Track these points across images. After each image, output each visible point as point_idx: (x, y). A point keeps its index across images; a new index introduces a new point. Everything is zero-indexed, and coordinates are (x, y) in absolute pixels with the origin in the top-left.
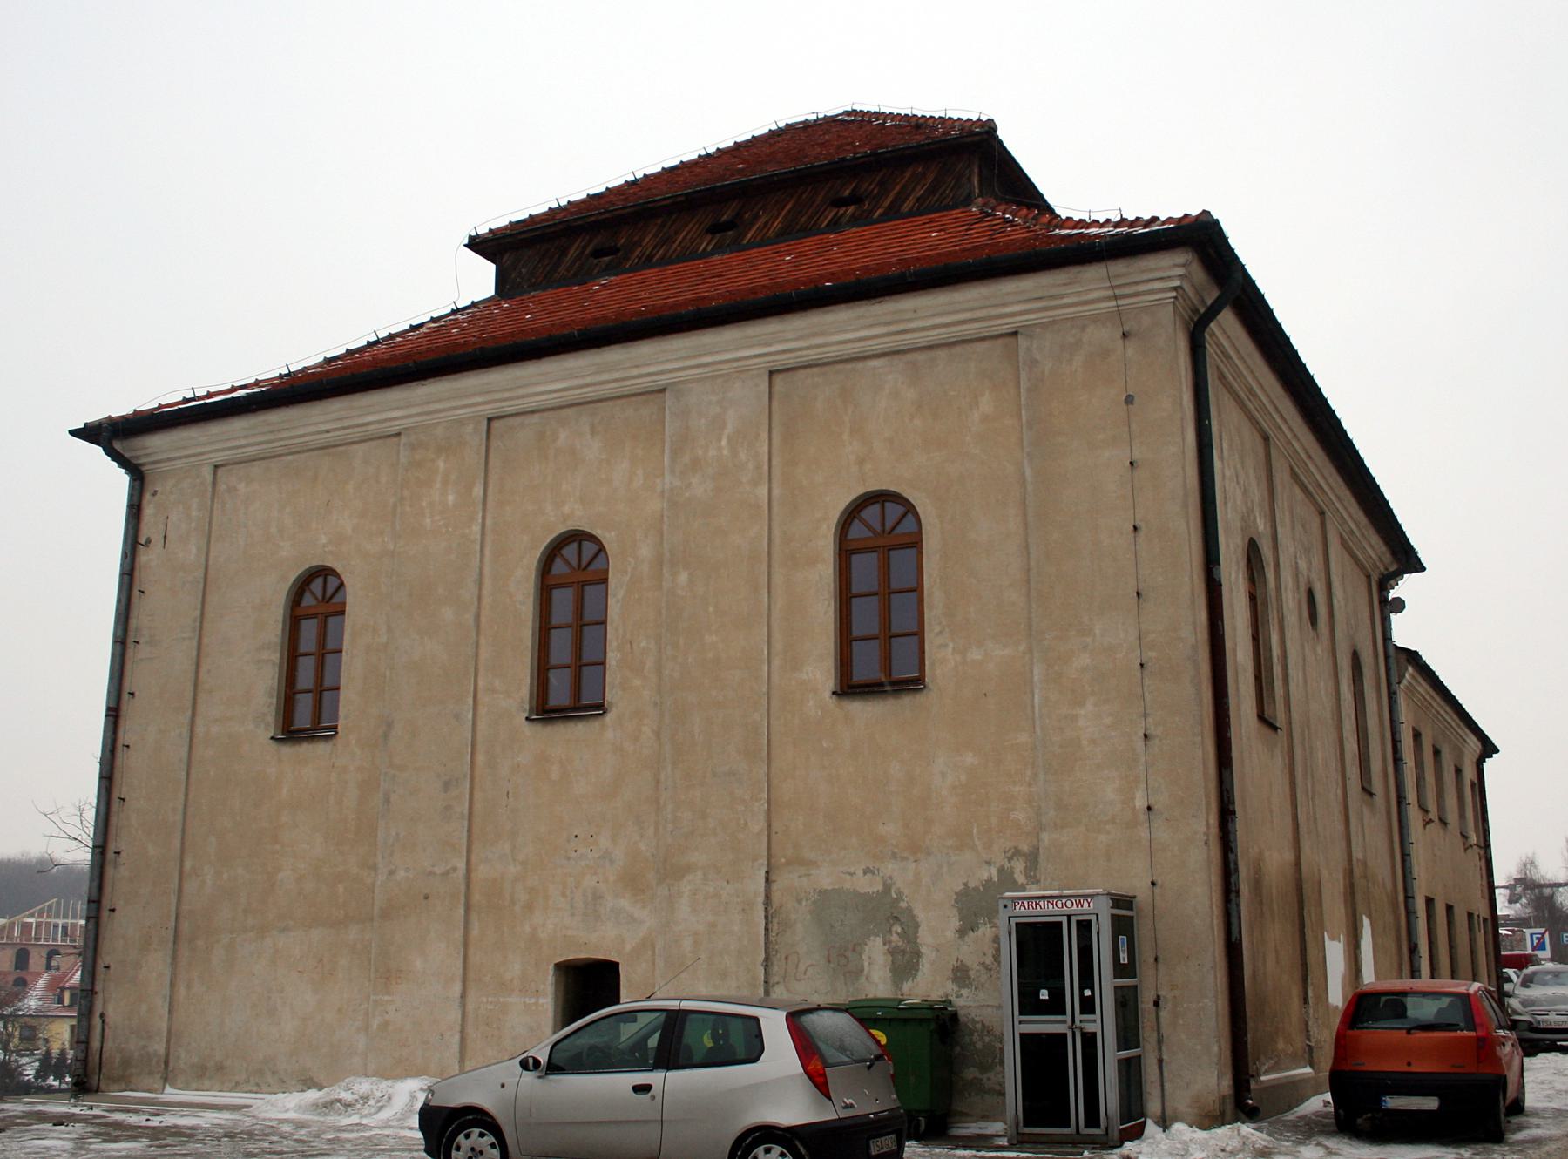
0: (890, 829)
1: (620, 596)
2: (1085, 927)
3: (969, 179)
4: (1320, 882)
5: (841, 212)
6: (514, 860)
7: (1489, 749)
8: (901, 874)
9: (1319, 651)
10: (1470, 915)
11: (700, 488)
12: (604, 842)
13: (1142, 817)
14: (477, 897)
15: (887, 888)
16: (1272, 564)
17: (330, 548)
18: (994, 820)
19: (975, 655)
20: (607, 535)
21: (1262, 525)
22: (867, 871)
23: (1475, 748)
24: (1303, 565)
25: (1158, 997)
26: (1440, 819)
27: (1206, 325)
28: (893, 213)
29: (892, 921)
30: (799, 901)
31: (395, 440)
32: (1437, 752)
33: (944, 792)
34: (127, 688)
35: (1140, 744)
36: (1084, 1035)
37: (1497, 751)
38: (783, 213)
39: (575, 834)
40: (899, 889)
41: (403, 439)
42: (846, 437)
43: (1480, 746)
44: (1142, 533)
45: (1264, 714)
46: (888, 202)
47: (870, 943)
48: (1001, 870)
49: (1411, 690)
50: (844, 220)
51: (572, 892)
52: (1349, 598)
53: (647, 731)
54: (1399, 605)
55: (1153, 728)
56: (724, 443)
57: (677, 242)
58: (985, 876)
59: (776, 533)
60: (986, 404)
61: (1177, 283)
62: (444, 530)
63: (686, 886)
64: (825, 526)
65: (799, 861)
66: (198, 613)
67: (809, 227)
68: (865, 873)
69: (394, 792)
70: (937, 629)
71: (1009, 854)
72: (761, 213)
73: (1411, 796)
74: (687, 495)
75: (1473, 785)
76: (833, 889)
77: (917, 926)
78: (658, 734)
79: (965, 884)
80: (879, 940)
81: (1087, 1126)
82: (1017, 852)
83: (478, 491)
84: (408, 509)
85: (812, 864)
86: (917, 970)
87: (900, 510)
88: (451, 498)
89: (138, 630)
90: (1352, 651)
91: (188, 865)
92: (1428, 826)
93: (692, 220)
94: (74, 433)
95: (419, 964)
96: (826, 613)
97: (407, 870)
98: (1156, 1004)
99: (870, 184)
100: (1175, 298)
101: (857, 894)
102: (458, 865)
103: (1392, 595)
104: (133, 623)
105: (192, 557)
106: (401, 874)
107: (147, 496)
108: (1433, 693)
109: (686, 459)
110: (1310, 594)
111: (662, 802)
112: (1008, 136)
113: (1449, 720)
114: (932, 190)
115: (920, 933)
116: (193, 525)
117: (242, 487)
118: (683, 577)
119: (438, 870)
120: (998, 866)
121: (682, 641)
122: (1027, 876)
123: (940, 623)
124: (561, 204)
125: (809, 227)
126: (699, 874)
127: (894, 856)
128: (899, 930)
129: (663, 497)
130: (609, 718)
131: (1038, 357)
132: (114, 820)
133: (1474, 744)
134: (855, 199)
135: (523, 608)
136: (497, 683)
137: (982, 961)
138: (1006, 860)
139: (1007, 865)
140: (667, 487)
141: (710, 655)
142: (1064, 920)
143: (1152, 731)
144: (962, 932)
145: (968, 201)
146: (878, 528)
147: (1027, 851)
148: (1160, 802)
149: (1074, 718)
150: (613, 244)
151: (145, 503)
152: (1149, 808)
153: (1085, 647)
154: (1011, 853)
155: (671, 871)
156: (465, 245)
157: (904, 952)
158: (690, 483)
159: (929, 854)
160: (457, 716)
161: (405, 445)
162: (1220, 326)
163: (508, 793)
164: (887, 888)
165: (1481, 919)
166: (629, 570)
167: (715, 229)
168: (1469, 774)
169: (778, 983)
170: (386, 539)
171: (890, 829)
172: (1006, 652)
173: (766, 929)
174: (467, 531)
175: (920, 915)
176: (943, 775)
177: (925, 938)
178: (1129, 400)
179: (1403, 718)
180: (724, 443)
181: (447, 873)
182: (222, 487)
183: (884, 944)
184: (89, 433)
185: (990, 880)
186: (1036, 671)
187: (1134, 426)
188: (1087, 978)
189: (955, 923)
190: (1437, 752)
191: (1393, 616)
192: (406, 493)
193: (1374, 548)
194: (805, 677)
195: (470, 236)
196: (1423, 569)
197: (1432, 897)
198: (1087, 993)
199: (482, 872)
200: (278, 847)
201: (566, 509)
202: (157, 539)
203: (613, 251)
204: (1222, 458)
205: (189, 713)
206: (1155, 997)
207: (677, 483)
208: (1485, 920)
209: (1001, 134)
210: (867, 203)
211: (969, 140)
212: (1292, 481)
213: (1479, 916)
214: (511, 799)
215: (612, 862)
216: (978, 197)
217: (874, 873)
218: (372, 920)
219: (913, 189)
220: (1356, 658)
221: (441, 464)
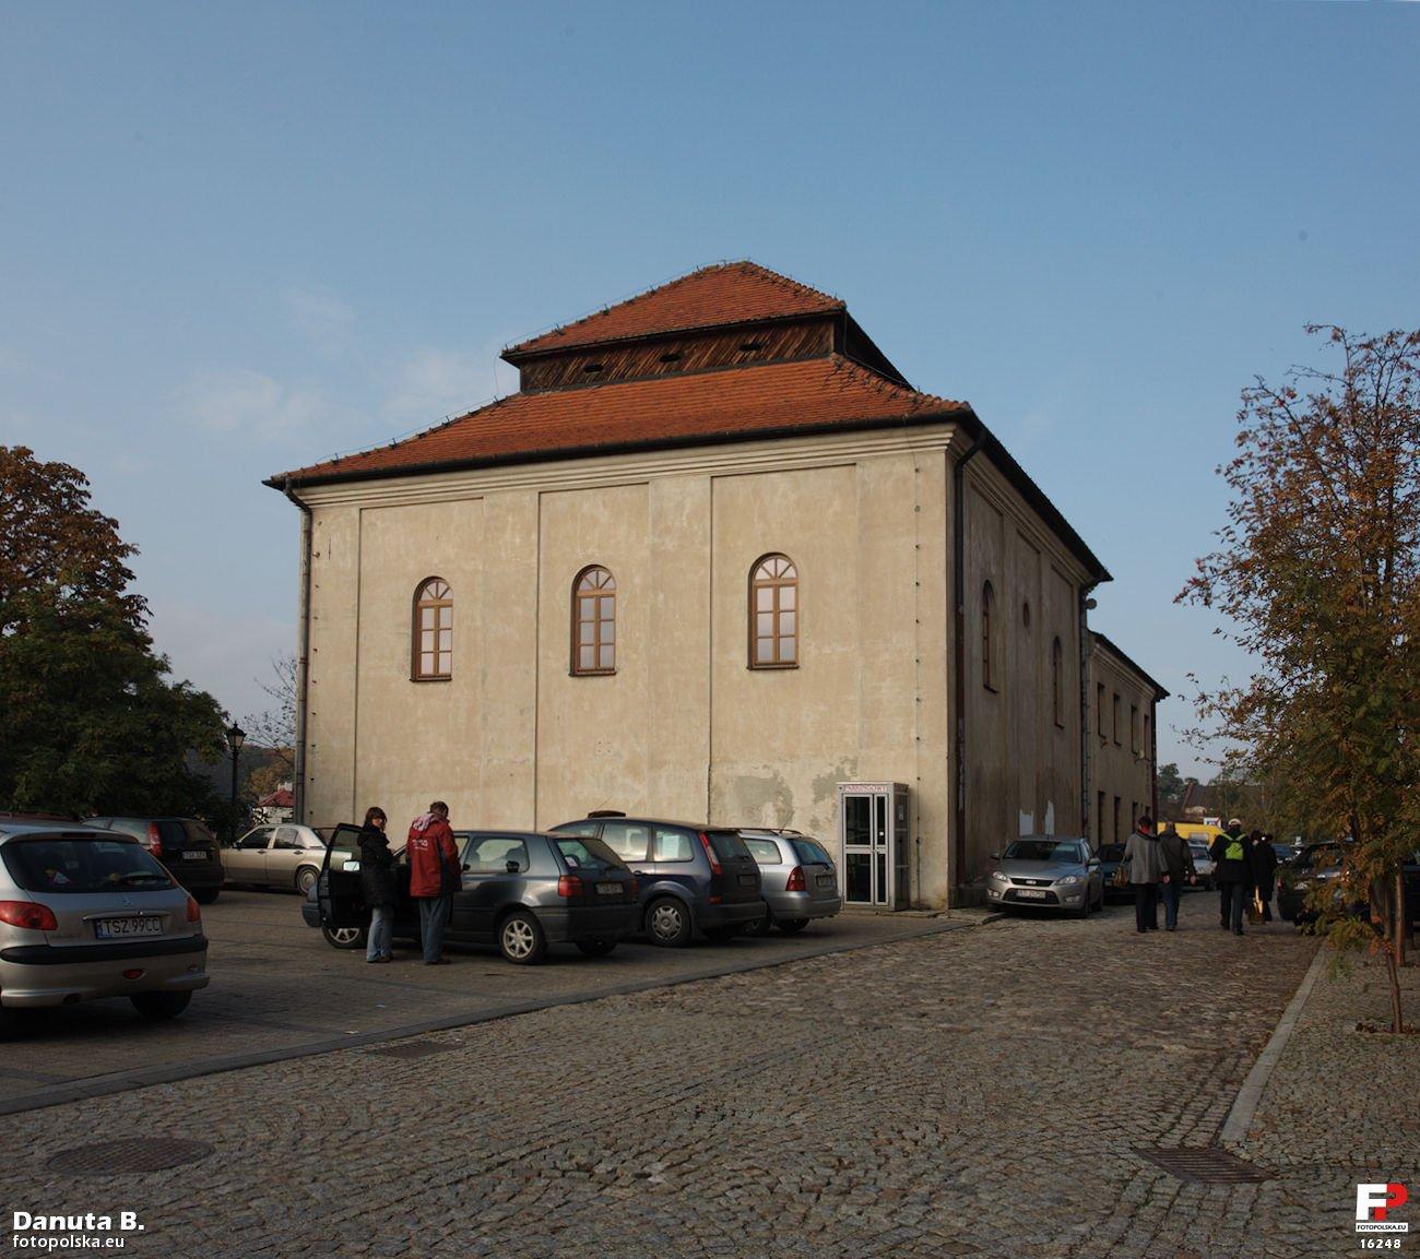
1: (624, 605)
2: (881, 801)
3: (828, 339)
7: (1161, 693)
10: (1135, 805)
11: (670, 544)
13: (914, 742)
15: (776, 776)
16: (1000, 593)
17: (441, 566)
19: (827, 650)
22: (765, 767)
24: (1022, 590)
27: (965, 462)
30: (727, 782)
32: (1116, 698)
34: (312, 645)
35: (914, 703)
36: (879, 855)
38: (710, 352)
42: (755, 520)
45: (988, 681)
46: (776, 350)
48: (838, 769)
50: (748, 360)
52: (1053, 596)
54: (1093, 604)
56: (684, 518)
58: (829, 772)
60: (837, 505)
61: (948, 442)
66: (356, 601)
70: (806, 635)
73: (1092, 727)
75: (1146, 717)
77: (791, 797)
80: (771, 804)
81: (879, 901)
82: (847, 759)
83: (534, 537)
84: (490, 545)
87: (786, 564)
88: (518, 540)
89: (316, 610)
90: (1053, 639)
91: (359, 753)
94: (263, 482)
95: (508, 813)
98: (918, 841)
101: (760, 780)
104: (313, 606)
106: (495, 762)
107: (315, 525)
110: (1026, 606)
112: (855, 312)
114: (802, 346)
115: (793, 801)
116: (348, 546)
117: (379, 524)
118: (661, 597)
127: (779, 759)
131: (867, 479)
132: (309, 726)
139: (841, 767)
141: (677, 643)
142: (871, 797)
143: (920, 698)
144: (815, 801)
145: (826, 353)
146: (773, 574)
148: (924, 735)
151: (314, 530)
153: (887, 650)
155: (656, 764)
160: (527, 673)
162: (974, 461)
164: (776, 776)
167: (666, 359)
168: (1143, 710)
172: (844, 650)
176: (808, 716)
177: (796, 803)
180: (684, 518)
181: (523, 762)
182: (365, 523)
184: (276, 483)
185: (832, 773)
188: (881, 826)
189: (813, 796)
190: (1116, 698)
191: (1088, 611)
193: (1076, 568)
196: (1112, 579)
198: (882, 834)
202: (324, 554)
203: (599, 368)
204: (970, 537)
205: (355, 663)
209: (849, 310)
215: (621, 757)
220: (1057, 642)
221: (510, 519)
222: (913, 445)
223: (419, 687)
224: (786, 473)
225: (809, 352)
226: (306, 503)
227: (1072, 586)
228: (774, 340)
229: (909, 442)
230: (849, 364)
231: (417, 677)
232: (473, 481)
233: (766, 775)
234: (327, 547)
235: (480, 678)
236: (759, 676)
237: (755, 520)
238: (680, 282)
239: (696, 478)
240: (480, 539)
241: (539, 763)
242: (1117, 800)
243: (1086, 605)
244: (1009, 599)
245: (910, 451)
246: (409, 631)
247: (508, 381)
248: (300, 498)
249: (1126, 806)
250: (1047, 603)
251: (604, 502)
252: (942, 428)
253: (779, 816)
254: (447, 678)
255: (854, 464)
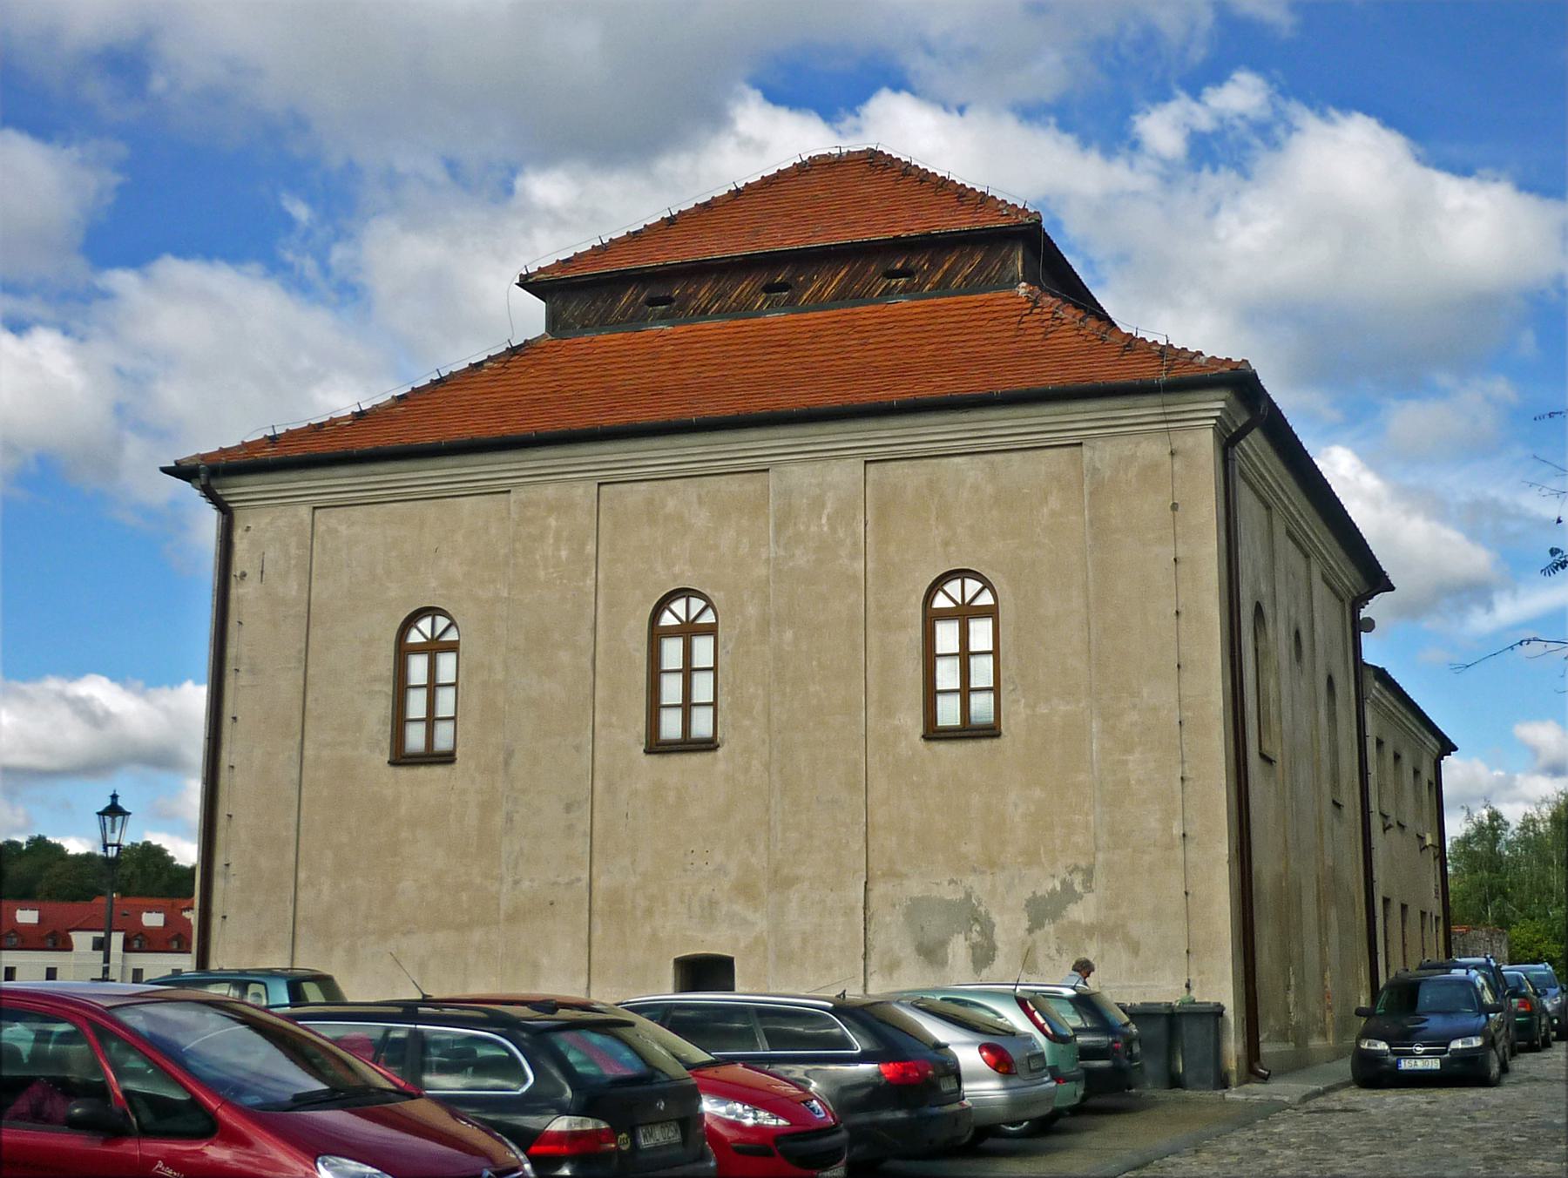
0: (971, 848)
4: (1300, 887)
5: (893, 283)
6: (634, 871)
7: (1448, 747)
8: (978, 885)
9: (1302, 684)
10: (1423, 914)
12: (719, 857)
13: (1179, 842)
14: (599, 903)
15: (969, 896)
18: (1058, 842)
19: (1043, 709)
20: (716, 594)
21: (1264, 588)
22: (951, 882)
23: (1433, 748)
25: (1189, 980)
26: (1399, 824)
28: (942, 288)
29: (972, 922)
31: (505, 495)
32: (1397, 757)
33: (1017, 819)
37: (1455, 749)
39: (692, 849)
40: (978, 896)
41: (513, 497)
42: (932, 522)
43: (1439, 747)
44: (1182, 617)
47: (954, 940)
48: (1063, 882)
49: (1377, 704)
51: (690, 898)
52: (1327, 620)
53: (756, 764)
54: (1369, 625)
55: (1188, 771)
56: (824, 520)
57: (732, 299)
58: (1050, 887)
59: (870, 599)
61: (1218, 414)
62: (558, 582)
63: (794, 895)
64: (914, 597)
65: (892, 874)
66: (304, 645)
67: (862, 295)
68: (949, 884)
69: (517, 812)
71: (1069, 869)
72: (815, 277)
74: (791, 564)
75: (1430, 783)
76: (923, 897)
78: (767, 767)
79: (1034, 893)
80: (961, 937)
83: (590, 548)
85: (905, 876)
86: (993, 960)
88: (564, 554)
89: (237, 659)
91: (302, 875)
92: (1387, 831)
93: (747, 277)
94: (165, 470)
96: (915, 670)
97: (532, 880)
99: (921, 260)
100: (1215, 425)
102: (582, 876)
103: (1364, 614)
105: (294, 593)
106: (526, 884)
108: (1396, 703)
109: (790, 532)
111: (772, 823)
113: (1410, 726)
114: (980, 269)
118: (789, 635)
119: (563, 880)
120: (1060, 879)
121: (788, 690)
122: (1085, 887)
123: (1013, 682)
124: (604, 242)
125: (862, 295)
126: (807, 884)
127: (974, 870)
128: (978, 929)
129: (769, 564)
130: (720, 752)
133: (1433, 744)
134: (906, 273)
135: (638, 655)
136: (614, 719)
137: (1047, 953)
138: (1067, 874)
139: (1068, 878)
140: (773, 555)
141: (814, 702)
143: (1188, 774)
147: (1084, 867)
149: (1126, 763)
150: (667, 294)
152: (1184, 835)
153: (1135, 706)
154: (1071, 868)
155: (782, 882)
156: (517, 284)
157: (982, 947)
158: (793, 555)
159: (1003, 868)
161: (515, 502)
163: (627, 815)
164: (969, 896)
165: (1434, 918)
166: (737, 626)
167: (770, 288)
168: (1427, 773)
169: (875, 972)
170: (498, 586)
171: (971, 848)
172: (1068, 707)
173: (865, 929)
174: (581, 584)
175: (996, 918)
176: (1016, 805)
177: (1000, 936)
178: (1174, 507)
179: (1368, 732)
180: (824, 520)
181: (570, 884)
183: (966, 940)
184: (181, 471)
185: (1054, 889)
186: (1094, 725)
187: (1178, 528)
189: (1026, 924)
190: (1397, 757)
192: (518, 546)
193: (1350, 577)
194: (897, 722)
195: (521, 275)
197: (1388, 897)
199: (601, 883)
200: (398, 859)
201: (677, 569)
202: (253, 574)
203: (668, 300)
205: (299, 737)
206: (1187, 980)
207: (782, 553)
208: (1437, 918)
210: (917, 277)
211: (1019, 229)
212: (1287, 537)
213: (1431, 914)
214: (630, 819)
215: (726, 874)
216: (1022, 281)
217: (956, 883)
218: (498, 923)
219: (962, 267)
222: (1169, 418)
223: (403, 772)
224: (977, 458)
225: (988, 279)
226: (226, 499)
227: (1342, 600)
228: (935, 266)
229: (1165, 414)
230: (1050, 299)
231: (401, 758)
232: (496, 468)
233: (952, 894)
234: (257, 563)
235: (501, 758)
236: (941, 748)
237: (932, 522)
238: (774, 177)
239: (842, 463)
240: (502, 552)
241: (595, 884)
242: (1404, 907)
243: (1360, 626)
244: (1282, 626)
245: (1165, 426)
246: (389, 689)
247: (530, 318)
248: (219, 492)
249: (1414, 913)
250: (1319, 628)
251: (699, 497)
252: (1212, 394)
253: (973, 955)
254: (448, 758)
255: (1081, 444)
